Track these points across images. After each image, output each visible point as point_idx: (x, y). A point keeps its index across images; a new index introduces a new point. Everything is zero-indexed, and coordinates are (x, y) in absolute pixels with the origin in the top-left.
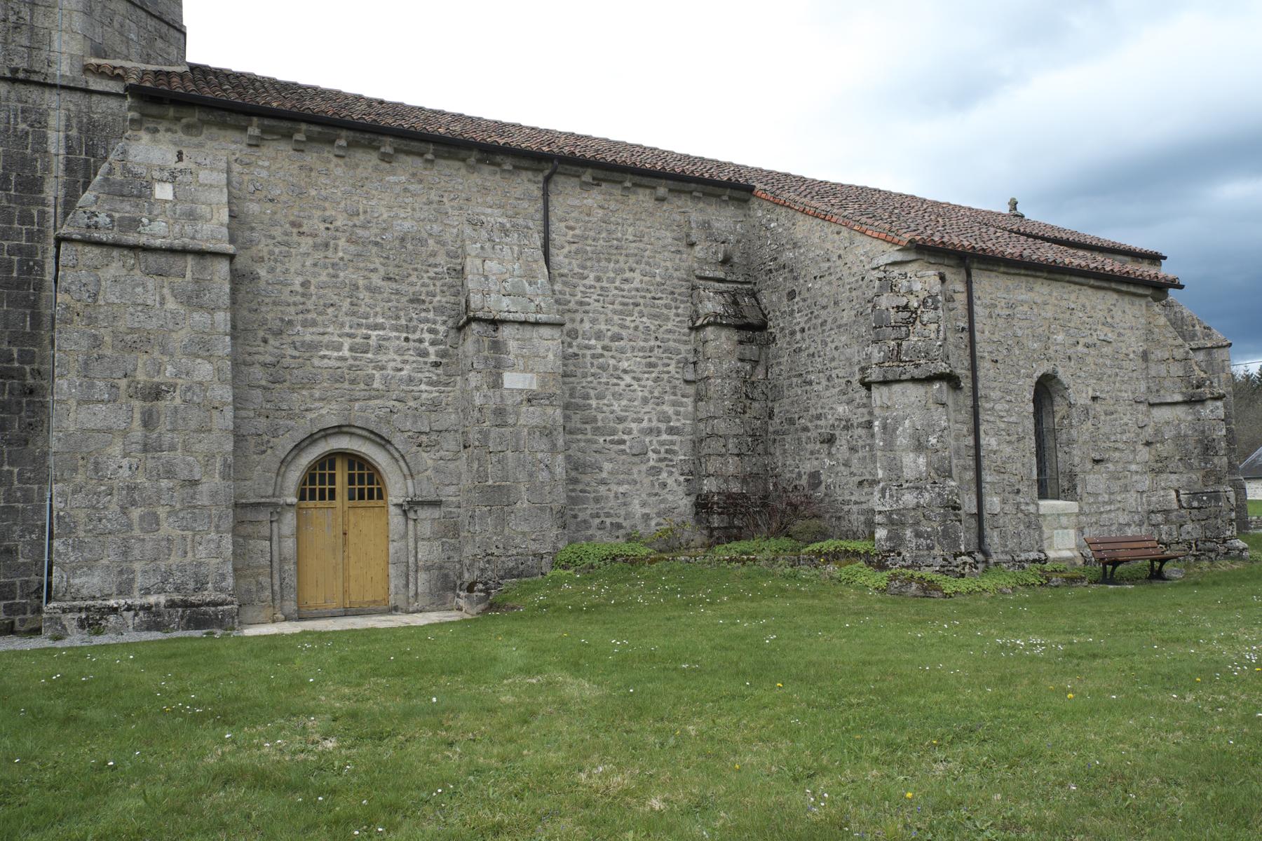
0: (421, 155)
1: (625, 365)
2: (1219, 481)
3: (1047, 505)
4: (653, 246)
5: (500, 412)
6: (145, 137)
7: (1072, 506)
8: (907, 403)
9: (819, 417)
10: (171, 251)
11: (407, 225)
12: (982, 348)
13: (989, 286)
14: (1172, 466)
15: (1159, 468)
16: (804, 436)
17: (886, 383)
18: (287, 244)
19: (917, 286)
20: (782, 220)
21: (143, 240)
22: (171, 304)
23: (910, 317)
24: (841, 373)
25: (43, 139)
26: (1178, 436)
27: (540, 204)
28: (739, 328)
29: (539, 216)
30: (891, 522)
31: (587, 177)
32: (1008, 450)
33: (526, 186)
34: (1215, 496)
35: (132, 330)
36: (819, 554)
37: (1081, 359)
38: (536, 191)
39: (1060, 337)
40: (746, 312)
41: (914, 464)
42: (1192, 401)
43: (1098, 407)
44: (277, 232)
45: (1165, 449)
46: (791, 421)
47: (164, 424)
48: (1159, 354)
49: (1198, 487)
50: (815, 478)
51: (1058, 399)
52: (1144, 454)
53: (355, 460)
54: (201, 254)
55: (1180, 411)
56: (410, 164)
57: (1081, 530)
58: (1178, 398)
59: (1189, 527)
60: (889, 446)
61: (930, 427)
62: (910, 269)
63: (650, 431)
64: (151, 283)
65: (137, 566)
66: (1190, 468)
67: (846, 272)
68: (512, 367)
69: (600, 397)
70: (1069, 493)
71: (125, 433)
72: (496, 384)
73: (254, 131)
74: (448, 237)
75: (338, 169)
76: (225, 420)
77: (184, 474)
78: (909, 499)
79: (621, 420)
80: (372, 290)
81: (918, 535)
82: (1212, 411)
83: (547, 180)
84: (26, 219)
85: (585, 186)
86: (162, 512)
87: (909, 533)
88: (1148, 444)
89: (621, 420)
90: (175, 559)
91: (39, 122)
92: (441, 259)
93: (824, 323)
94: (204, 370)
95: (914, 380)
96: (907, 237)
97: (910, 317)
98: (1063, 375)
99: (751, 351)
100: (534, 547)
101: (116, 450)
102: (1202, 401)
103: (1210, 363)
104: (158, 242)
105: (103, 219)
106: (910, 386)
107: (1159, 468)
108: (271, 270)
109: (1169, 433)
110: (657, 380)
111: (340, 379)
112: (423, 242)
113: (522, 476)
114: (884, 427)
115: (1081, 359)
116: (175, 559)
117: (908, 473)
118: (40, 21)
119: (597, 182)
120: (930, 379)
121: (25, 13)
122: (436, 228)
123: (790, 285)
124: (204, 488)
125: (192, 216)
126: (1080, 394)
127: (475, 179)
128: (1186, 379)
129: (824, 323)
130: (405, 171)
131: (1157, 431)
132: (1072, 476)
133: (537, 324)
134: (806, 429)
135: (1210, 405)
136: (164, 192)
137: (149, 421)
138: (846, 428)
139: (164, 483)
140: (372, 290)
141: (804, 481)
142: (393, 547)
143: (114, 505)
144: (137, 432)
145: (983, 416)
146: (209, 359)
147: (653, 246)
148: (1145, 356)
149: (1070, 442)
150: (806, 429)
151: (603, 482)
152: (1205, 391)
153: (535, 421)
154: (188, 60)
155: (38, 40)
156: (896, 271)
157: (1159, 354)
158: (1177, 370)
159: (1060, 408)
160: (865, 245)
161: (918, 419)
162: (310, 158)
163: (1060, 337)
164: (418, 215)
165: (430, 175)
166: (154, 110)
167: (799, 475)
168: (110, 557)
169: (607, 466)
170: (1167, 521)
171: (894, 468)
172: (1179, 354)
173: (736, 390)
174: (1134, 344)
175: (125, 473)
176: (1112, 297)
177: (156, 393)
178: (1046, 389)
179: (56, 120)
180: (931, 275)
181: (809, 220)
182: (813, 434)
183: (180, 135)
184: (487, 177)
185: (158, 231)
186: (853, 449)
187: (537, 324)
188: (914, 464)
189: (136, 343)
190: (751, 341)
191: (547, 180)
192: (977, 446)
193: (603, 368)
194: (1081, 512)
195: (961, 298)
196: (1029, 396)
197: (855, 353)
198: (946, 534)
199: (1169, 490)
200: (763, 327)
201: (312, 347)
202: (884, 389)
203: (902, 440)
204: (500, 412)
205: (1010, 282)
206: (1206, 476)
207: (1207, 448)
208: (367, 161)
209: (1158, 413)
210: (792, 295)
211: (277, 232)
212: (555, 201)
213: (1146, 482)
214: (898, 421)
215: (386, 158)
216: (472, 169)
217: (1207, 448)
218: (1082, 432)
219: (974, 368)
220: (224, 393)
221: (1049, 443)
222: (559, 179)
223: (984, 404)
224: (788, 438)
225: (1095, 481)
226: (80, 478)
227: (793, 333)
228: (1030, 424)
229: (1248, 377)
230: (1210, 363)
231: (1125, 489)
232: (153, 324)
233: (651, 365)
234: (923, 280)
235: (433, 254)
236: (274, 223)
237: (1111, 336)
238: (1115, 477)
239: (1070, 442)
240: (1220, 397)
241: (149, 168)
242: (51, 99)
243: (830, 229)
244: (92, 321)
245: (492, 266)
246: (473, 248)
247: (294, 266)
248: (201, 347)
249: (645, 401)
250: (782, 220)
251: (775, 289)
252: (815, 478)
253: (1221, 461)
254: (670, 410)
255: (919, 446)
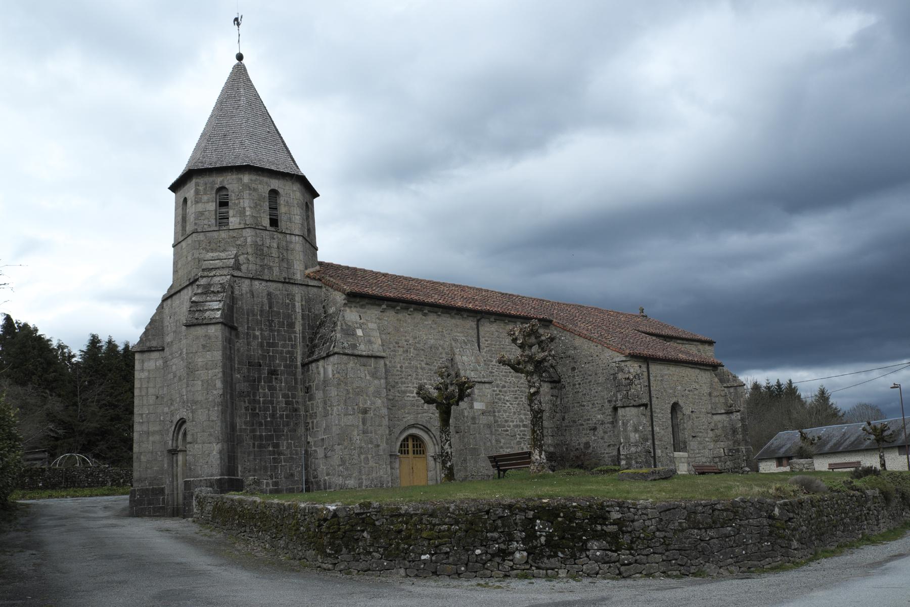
0: (436, 313)
1: (507, 398)
2: (739, 445)
3: (677, 454)
4: (500, 340)
5: (473, 418)
6: (348, 310)
7: (685, 454)
8: (630, 415)
9: (588, 420)
10: (368, 357)
11: (432, 341)
12: (653, 393)
13: (655, 369)
14: (721, 439)
15: (716, 440)
16: (581, 428)
17: (624, 407)
18: (394, 351)
19: (632, 370)
20: (568, 337)
21: (360, 353)
22: (368, 378)
23: (630, 382)
24: (599, 402)
25: (294, 306)
26: (723, 427)
27: (476, 331)
28: (551, 382)
29: (475, 336)
30: (627, 458)
31: (492, 319)
32: (663, 432)
33: (470, 323)
34: (738, 451)
35: (358, 387)
36: (601, 471)
37: (687, 396)
38: (474, 324)
39: (679, 388)
40: (553, 375)
41: (634, 437)
42: (728, 413)
43: (694, 415)
44: (391, 346)
45: (718, 432)
46: (574, 422)
47: (368, 424)
48: (715, 394)
49: (731, 447)
50: (587, 445)
51: (679, 412)
52: (711, 434)
53: (415, 437)
54: (376, 357)
55: (724, 417)
56: (432, 317)
57: (689, 464)
58: (723, 411)
59: (728, 463)
60: (625, 430)
61: (640, 423)
62: (628, 363)
63: (517, 426)
64: (362, 368)
65: (364, 477)
66: (728, 439)
67: (600, 362)
68: (477, 401)
69: (499, 412)
70: (684, 449)
71: (358, 426)
72: (472, 407)
73: (384, 306)
74: (445, 346)
75: (409, 319)
76: (385, 422)
77: (375, 443)
78: (633, 449)
79: (506, 421)
80: (422, 369)
81: (637, 463)
82: (736, 416)
83: (478, 321)
84: (290, 339)
85: (491, 322)
86: (370, 456)
87: (633, 462)
88: (712, 430)
89: (506, 421)
90: (374, 475)
91: (291, 297)
92: (444, 355)
93: (590, 382)
94: (379, 402)
95: (634, 406)
96: (628, 351)
97: (630, 382)
98: (681, 403)
99: (555, 392)
100: (486, 472)
101: (355, 433)
102: (732, 413)
103: (736, 393)
104: (364, 353)
105: (346, 345)
106: (633, 409)
107: (716, 440)
108: (390, 362)
109: (720, 426)
110: (518, 404)
111: (413, 405)
112: (438, 349)
113: (482, 444)
114: (623, 423)
115: (687, 396)
116: (374, 475)
117: (632, 440)
118: (290, 257)
119: (496, 320)
120: (639, 406)
121: (285, 254)
122: (442, 342)
123: (572, 365)
124: (381, 448)
125: (370, 342)
126: (687, 410)
127: (453, 321)
128: (726, 403)
129: (590, 382)
130: (430, 320)
131: (716, 425)
132: (685, 443)
133: (485, 383)
134: (582, 425)
135: (735, 414)
136: (359, 332)
137: (364, 423)
138: (602, 424)
139: (370, 446)
140: (422, 369)
141: (582, 446)
142: (430, 474)
143: (356, 452)
144: (361, 427)
145: (654, 419)
146: (380, 398)
147: (500, 340)
148: (710, 394)
149: (684, 429)
150: (582, 425)
151: (502, 448)
152: (733, 409)
153: (485, 422)
154: (320, 259)
155: (290, 266)
156: (623, 364)
157: (715, 394)
158: (722, 400)
159: (680, 416)
160: (608, 353)
161: (635, 420)
162: (400, 316)
163: (679, 388)
164: (436, 337)
165: (439, 320)
166: (352, 300)
167: (579, 444)
168: (356, 474)
169: (503, 441)
170: (720, 461)
171: (627, 438)
172: (723, 393)
173: (550, 409)
174: (706, 390)
175: (358, 442)
176: (697, 371)
177: (365, 411)
178: (675, 407)
179: (298, 298)
180: (636, 365)
181: (582, 340)
182: (585, 427)
183: (359, 309)
184: (457, 321)
185: (362, 349)
186: (605, 432)
187: (485, 383)
188: (634, 437)
189: (359, 392)
190: (555, 388)
191: (478, 321)
192: (653, 430)
193: (500, 399)
194: (689, 457)
195: (645, 374)
196: (669, 411)
197: (606, 395)
198: (647, 462)
199: (721, 449)
200: (559, 382)
201: (405, 392)
202: (623, 409)
203: (630, 428)
204: (473, 418)
205: (661, 367)
206: (734, 443)
207: (734, 431)
208: (418, 316)
209: (715, 417)
210: (573, 369)
211: (391, 346)
212: (481, 329)
213: (712, 446)
214: (628, 421)
215: (425, 315)
216: (452, 317)
217: (734, 431)
218: (688, 425)
219: (651, 400)
220: (384, 411)
221: (676, 429)
222: (483, 320)
223: (655, 415)
224: (573, 429)
225: (693, 445)
226: (346, 444)
227: (574, 385)
228: (670, 422)
229: (768, 388)
230: (736, 393)
231: (704, 448)
232: (363, 385)
233: (516, 398)
234: (634, 368)
235: (441, 353)
236: (391, 343)
237: (698, 387)
238: (700, 443)
239: (684, 429)
240: (739, 411)
241: (353, 323)
242: (296, 290)
243: (592, 344)
244: (346, 384)
245: (464, 358)
246: (457, 351)
247: (397, 360)
248: (377, 394)
249: (515, 413)
250: (568, 337)
251: (565, 365)
252: (587, 445)
253: (740, 437)
254: (523, 417)
255: (636, 430)
